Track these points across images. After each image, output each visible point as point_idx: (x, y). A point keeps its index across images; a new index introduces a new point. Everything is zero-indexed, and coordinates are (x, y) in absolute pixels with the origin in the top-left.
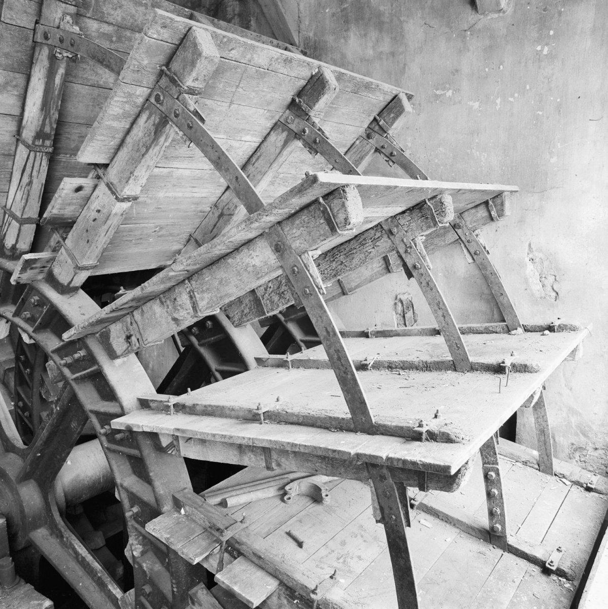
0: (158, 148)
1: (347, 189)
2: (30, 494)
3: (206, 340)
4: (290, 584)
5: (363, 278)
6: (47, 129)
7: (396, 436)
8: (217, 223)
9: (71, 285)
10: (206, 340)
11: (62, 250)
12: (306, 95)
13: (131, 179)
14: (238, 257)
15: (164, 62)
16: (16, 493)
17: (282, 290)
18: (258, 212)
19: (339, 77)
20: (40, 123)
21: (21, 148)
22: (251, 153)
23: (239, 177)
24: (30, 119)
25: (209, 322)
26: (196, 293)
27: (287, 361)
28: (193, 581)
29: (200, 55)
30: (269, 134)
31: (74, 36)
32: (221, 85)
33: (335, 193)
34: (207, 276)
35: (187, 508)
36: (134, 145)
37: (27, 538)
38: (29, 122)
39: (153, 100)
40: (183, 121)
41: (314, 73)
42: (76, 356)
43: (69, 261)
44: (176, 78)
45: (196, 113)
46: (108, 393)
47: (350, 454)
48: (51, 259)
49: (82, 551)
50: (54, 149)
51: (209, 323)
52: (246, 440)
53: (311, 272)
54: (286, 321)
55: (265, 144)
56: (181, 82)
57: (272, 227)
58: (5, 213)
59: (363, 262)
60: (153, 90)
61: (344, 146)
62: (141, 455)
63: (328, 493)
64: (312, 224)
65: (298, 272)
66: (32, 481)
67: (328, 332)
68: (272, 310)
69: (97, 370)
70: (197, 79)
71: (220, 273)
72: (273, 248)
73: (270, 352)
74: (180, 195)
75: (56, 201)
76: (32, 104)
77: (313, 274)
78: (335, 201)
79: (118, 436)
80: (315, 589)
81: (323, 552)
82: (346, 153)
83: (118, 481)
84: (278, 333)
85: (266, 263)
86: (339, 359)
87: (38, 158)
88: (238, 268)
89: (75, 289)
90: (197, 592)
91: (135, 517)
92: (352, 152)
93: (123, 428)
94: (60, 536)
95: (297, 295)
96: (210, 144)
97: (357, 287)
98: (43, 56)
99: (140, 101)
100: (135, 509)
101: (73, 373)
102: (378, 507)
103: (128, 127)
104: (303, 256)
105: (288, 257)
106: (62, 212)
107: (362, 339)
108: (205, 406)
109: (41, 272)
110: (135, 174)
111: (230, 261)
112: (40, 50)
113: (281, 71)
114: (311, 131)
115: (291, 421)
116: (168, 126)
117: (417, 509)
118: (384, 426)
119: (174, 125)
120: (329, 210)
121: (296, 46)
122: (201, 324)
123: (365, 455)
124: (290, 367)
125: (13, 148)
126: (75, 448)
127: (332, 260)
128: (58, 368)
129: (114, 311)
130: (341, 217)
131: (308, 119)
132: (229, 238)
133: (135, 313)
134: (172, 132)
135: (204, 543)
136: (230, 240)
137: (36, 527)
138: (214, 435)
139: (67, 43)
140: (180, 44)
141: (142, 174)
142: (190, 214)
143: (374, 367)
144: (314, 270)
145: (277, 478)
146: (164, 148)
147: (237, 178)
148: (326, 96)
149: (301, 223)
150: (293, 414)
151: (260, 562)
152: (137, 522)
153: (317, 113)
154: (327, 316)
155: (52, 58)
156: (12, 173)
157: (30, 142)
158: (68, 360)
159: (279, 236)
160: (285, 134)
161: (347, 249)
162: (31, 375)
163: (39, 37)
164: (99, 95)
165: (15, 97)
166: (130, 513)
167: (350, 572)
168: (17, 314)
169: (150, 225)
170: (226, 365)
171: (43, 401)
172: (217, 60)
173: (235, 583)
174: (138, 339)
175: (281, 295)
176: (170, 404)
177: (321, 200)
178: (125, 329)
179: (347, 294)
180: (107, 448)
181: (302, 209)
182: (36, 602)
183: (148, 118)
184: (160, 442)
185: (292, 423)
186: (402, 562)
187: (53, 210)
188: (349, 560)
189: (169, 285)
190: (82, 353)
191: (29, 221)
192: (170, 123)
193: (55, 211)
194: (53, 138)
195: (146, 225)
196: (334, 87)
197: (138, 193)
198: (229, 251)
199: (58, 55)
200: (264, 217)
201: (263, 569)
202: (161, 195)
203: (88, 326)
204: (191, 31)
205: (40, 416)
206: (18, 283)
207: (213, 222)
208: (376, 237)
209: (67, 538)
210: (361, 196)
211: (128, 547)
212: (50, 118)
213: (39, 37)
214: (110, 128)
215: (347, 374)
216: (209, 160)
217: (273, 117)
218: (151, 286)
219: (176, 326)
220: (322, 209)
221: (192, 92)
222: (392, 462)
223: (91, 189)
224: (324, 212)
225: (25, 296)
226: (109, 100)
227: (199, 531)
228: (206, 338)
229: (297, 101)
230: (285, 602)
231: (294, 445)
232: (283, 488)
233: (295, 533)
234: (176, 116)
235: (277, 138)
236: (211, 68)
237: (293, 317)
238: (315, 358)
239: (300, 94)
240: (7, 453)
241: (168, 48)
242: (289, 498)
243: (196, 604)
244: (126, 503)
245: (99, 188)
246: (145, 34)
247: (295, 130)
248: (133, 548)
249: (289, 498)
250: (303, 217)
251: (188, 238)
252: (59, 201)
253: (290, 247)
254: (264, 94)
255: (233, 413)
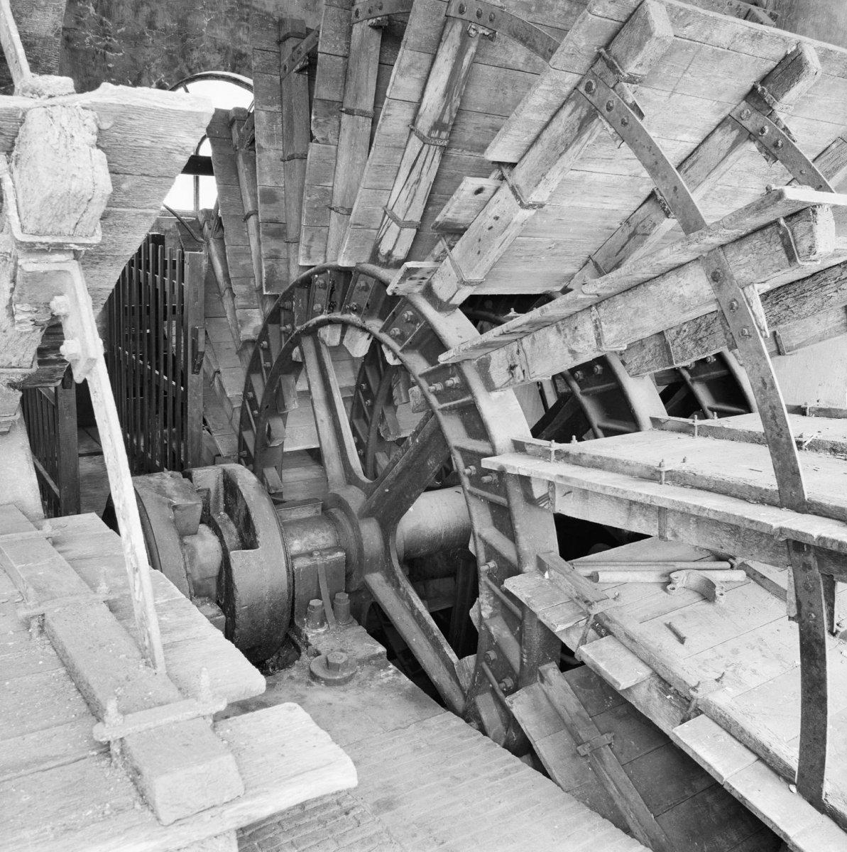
0: (578, 147)
1: (818, 210)
2: (370, 533)
3: (591, 389)
4: (665, 676)
5: (810, 335)
6: (446, 119)
7: (833, 519)
8: (626, 244)
9: (451, 302)
10: (591, 389)
11: (447, 260)
12: (773, 82)
13: (541, 183)
14: (662, 284)
15: (603, 43)
16: (356, 528)
17: (701, 336)
18: (701, 231)
19: (825, 56)
20: (440, 111)
21: (414, 139)
22: (684, 157)
23: (679, 188)
24: (429, 107)
25: (598, 366)
26: (603, 323)
27: (693, 426)
28: (545, 657)
29: (650, 35)
30: (713, 132)
31: (494, 9)
32: (666, 70)
33: (802, 213)
34: (620, 304)
35: (553, 572)
36: (551, 142)
37: (362, 580)
38: (427, 111)
39: (582, 89)
40: (617, 115)
41: (789, 53)
42: (449, 383)
43: (454, 273)
44: (616, 63)
45: (635, 107)
46: (478, 428)
47: (772, 526)
48: (432, 271)
49: (420, 605)
50: (449, 143)
51: (599, 367)
52: (643, 497)
53: (754, 309)
54: (692, 381)
55: (706, 145)
56: (621, 67)
57: (712, 250)
58: (385, 213)
59: (819, 309)
60: (584, 76)
61: (812, 151)
62: (509, 503)
63: (723, 592)
64: (765, 250)
65: (737, 308)
66: (374, 519)
67: (764, 384)
68: (683, 359)
69: (470, 401)
70: (641, 65)
71: (637, 301)
72: (710, 277)
73: (670, 414)
74: (588, 205)
75: (452, 204)
76: (434, 89)
77: (756, 312)
78: (801, 224)
79: (486, 479)
80: (697, 686)
81: (708, 655)
82: (814, 160)
83: (477, 530)
84: (680, 395)
85: (697, 294)
86: (774, 417)
87: (431, 152)
88: (661, 297)
89: (454, 307)
90: (548, 670)
91: (490, 574)
92: (823, 161)
93: (496, 469)
94: (397, 585)
95: (731, 336)
96: (647, 145)
97: (799, 346)
98: (455, 32)
99: (567, 89)
100: (492, 564)
101: (441, 402)
102: (795, 602)
103: (547, 120)
104: (746, 289)
105: (726, 288)
106: (457, 216)
107: (795, 415)
108: (594, 457)
109: (420, 284)
110: (547, 177)
111: (652, 287)
112: (452, 26)
113: (746, 51)
114: (773, 131)
115: (699, 486)
116: (596, 121)
117: (840, 638)
118: (820, 504)
119: (604, 121)
120: (790, 234)
121: (762, 6)
122: (587, 367)
123: (791, 530)
124: (696, 433)
125: (405, 140)
126: (424, 495)
127: (774, 302)
128: (424, 396)
129: (504, 334)
130: (804, 245)
131: (770, 114)
132: (659, 259)
133: (524, 340)
134: (600, 128)
135: (569, 613)
136: (659, 262)
137: (372, 571)
138: (604, 488)
139: (485, 18)
140: (627, 21)
141: (555, 176)
142: (594, 229)
143: (810, 447)
144: (758, 308)
145: (661, 563)
146: (585, 148)
147: (676, 188)
148: (801, 83)
149: (751, 248)
150: (703, 478)
151: (632, 644)
152: (491, 579)
153: (785, 106)
154: (767, 364)
155: (465, 35)
156: (399, 168)
157: (425, 134)
158: (439, 387)
159: (719, 262)
160: (735, 133)
161: (798, 290)
162: (371, 407)
163: (453, 10)
164: (505, 78)
165: (417, 81)
166: (486, 568)
167: (740, 682)
168: (384, 330)
169: (545, 240)
170: (612, 423)
171: (380, 439)
172: (669, 41)
173: (602, 660)
174: (524, 371)
175: (698, 342)
176: (551, 449)
177: (782, 222)
178: (509, 357)
179: (784, 354)
180: (469, 492)
181: (755, 231)
182: (369, 645)
183: (573, 111)
184: (532, 493)
185: (699, 488)
186: (815, 671)
187: (449, 213)
188: (741, 671)
189: (573, 310)
190: (456, 380)
191: (409, 224)
192: (600, 117)
193: (449, 215)
194: (450, 128)
195: (540, 239)
196: (815, 71)
197: (545, 199)
198: (653, 276)
199: (473, 32)
200: (707, 237)
201: (634, 653)
202: (566, 204)
203: (470, 348)
204: (644, 4)
205: (375, 456)
206: (394, 294)
207: (620, 243)
208: (843, 277)
209: (404, 589)
210: (835, 219)
211: (475, 606)
212: (451, 106)
213: (453, 10)
214: (528, 121)
215: (781, 437)
216: (643, 164)
217: (722, 110)
218: (550, 310)
219: (572, 359)
220: (781, 233)
221: (632, 80)
222: (824, 543)
223: (492, 192)
224: (784, 237)
225: (398, 309)
226: (532, 89)
227: (564, 599)
228: (592, 386)
229: (759, 89)
230: (656, 695)
231: (702, 509)
232: (668, 575)
233: (676, 626)
234: (608, 110)
235: (724, 138)
236: (660, 50)
237: (703, 376)
238: (731, 427)
239: (764, 80)
240: (349, 486)
241: (611, 26)
242: (674, 589)
243: (546, 682)
244: (482, 557)
245: (501, 190)
246: (589, 11)
247: (750, 129)
248: (482, 607)
249: (674, 589)
250: (755, 242)
251: (585, 259)
252: (456, 204)
253: (732, 277)
254: (716, 80)
255: (627, 468)
